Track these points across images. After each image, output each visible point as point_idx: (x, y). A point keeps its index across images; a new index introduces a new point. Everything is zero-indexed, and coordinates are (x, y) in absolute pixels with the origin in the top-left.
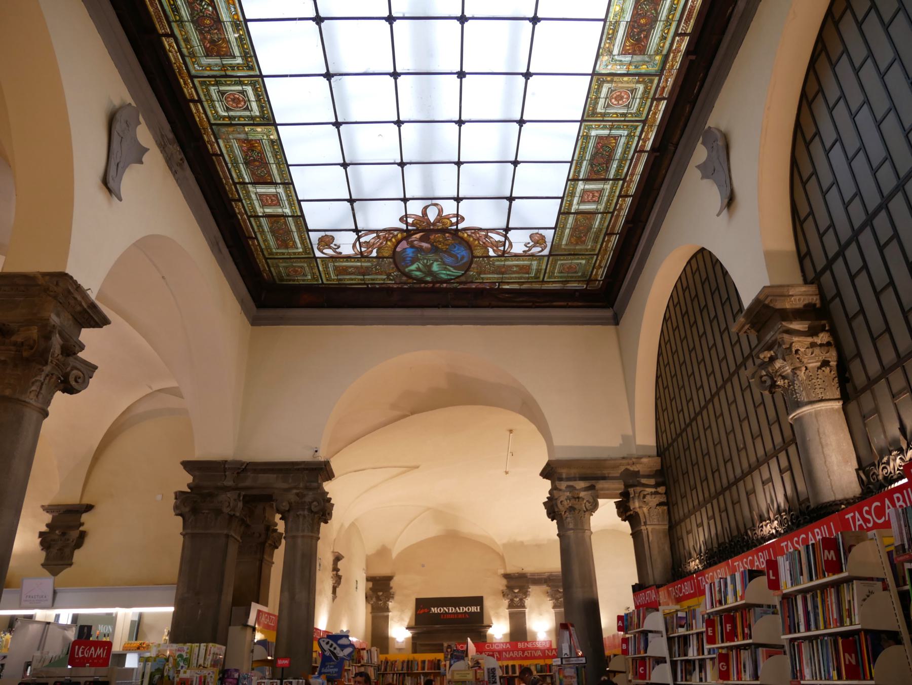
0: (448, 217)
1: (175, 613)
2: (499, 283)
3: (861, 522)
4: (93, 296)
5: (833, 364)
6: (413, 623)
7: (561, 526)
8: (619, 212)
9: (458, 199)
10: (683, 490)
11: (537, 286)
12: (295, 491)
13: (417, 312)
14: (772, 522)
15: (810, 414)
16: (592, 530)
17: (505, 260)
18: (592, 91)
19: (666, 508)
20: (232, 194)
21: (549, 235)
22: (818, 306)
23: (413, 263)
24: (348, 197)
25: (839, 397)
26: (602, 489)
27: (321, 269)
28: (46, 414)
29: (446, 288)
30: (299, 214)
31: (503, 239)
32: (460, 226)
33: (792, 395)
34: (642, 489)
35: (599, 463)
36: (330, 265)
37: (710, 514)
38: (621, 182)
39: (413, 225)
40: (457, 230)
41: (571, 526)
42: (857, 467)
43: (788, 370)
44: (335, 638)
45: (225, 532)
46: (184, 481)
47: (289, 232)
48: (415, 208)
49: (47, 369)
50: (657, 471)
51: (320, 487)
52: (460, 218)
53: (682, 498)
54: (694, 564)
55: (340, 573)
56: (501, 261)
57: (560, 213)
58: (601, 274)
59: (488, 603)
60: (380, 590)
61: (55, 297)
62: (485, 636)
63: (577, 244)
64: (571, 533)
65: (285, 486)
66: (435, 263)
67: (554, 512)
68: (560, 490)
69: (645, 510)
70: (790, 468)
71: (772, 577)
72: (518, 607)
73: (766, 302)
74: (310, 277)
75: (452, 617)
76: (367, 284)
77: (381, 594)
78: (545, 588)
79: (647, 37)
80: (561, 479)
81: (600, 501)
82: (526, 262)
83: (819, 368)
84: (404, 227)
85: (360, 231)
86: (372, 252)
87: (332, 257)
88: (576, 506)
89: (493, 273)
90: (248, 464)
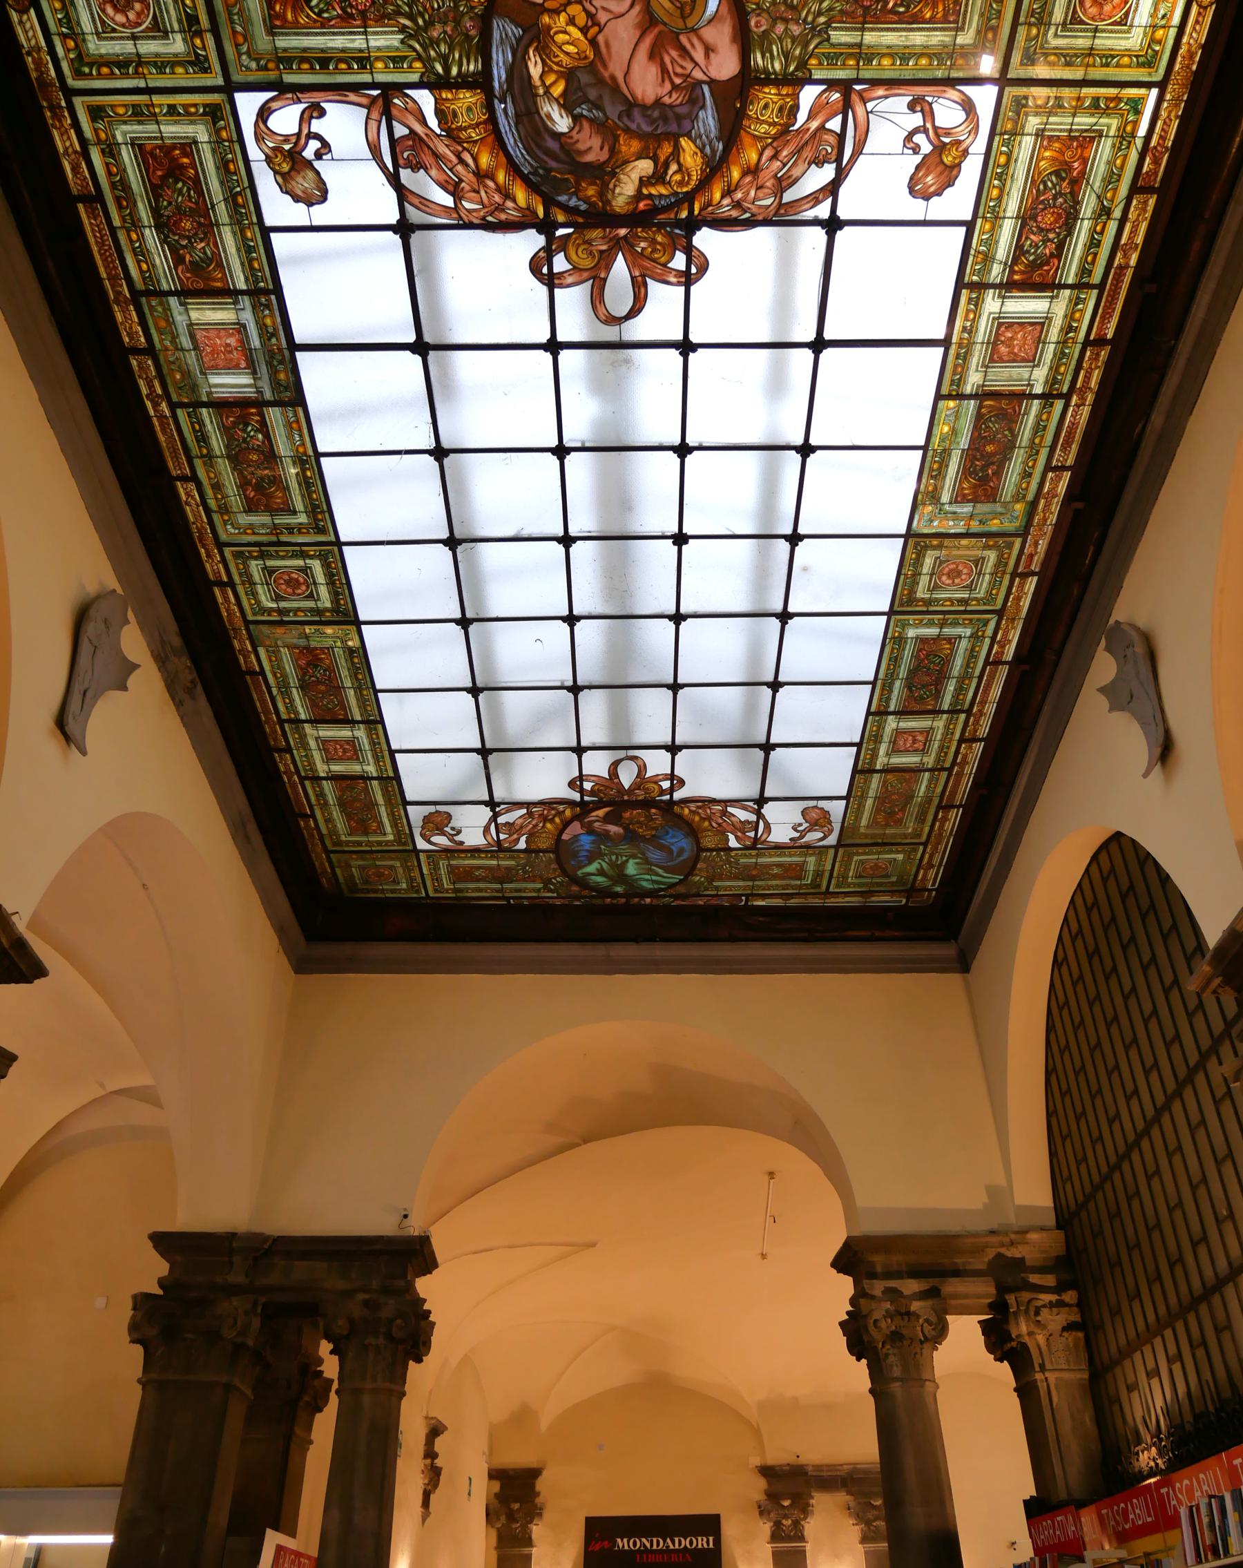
0: (655, 780)
2: (747, 896)
7: (876, 1373)
9: (673, 749)
11: (815, 902)
12: (362, 1296)
13: (598, 951)
17: (757, 856)
18: (907, 563)
21: (837, 809)
24: (479, 745)
30: (391, 774)
31: (753, 818)
32: (677, 795)
36: (443, 864)
37: (1172, 1350)
38: (963, 716)
39: (592, 793)
40: (671, 802)
46: (150, 1272)
47: (372, 805)
48: (597, 764)
50: (1058, 1258)
56: (751, 856)
57: (855, 771)
58: (932, 878)
59: (729, 1530)
63: (887, 825)
65: (341, 1285)
66: (631, 862)
68: (873, 1297)
69: (1041, 1339)
76: (508, 899)
77: (516, 1506)
78: (842, 1497)
79: (998, 474)
80: (873, 1276)
84: (576, 796)
85: (499, 804)
88: (905, 1332)
89: (736, 878)
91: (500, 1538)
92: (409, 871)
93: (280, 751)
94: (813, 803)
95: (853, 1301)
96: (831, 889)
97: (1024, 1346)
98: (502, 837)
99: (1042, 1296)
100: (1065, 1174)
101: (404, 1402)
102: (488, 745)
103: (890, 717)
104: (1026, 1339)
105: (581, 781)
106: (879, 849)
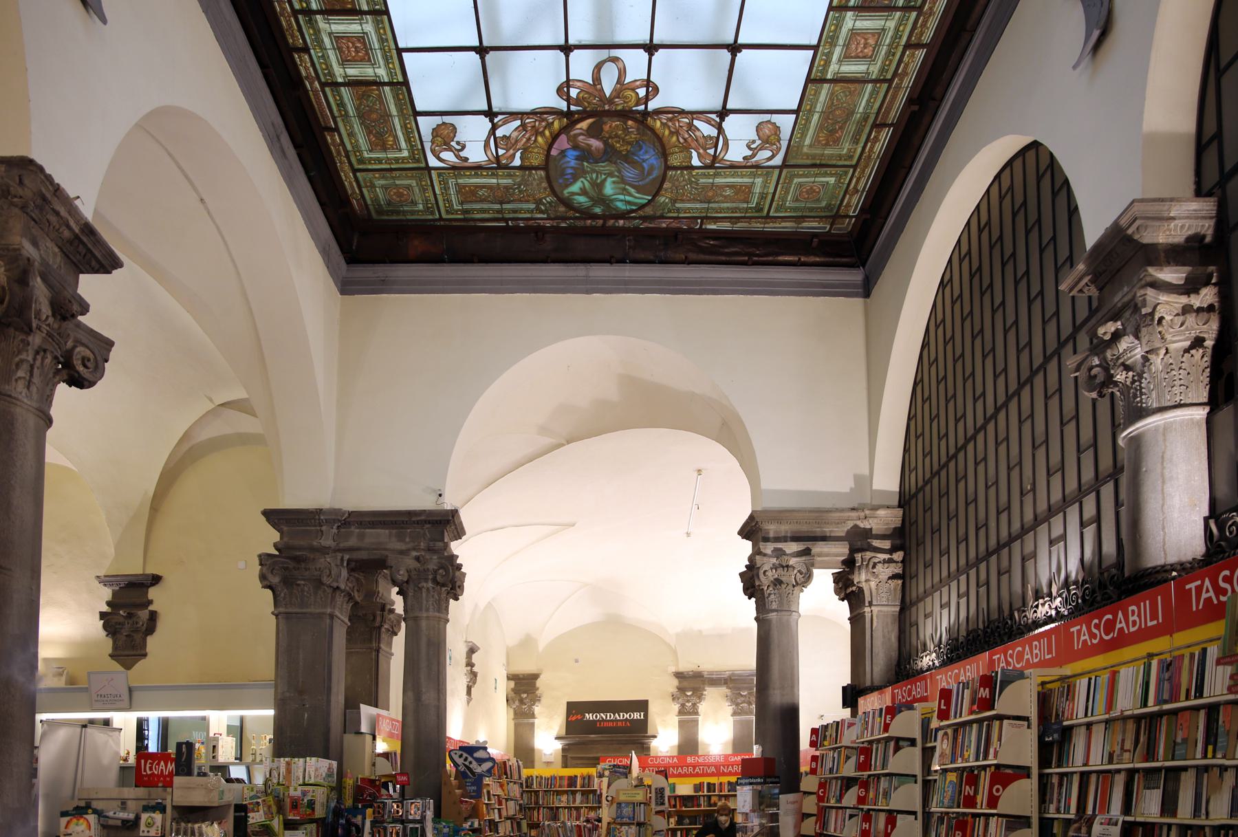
0: (633, 87)
1: (277, 719)
2: (702, 218)
3: (1087, 637)
4: (87, 211)
5: (1209, 343)
6: (563, 733)
7: (761, 608)
8: (901, 80)
9: (651, 48)
10: (928, 557)
11: (757, 226)
12: (414, 554)
13: (579, 271)
14: (1052, 598)
15: (1156, 429)
16: (801, 610)
17: (715, 175)
19: (900, 582)
20: (293, 36)
22: (1208, 239)
23: (575, 180)
24: (477, 44)
25: (1206, 400)
26: (820, 555)
27: (438, 192)
28: (49, 422)
29: (623, 229)
30: (401, 79)
31: (714, 132)
32: (653, 105)
33: (1135, 396)
34: (872, 554)
35: (820, 514)
36: (451, 182)
37: (963, 589)
38: (914, 14)
39: (578, 102)
40: (646, 113)
41: (774, 606)
42: (1207, 514)
43: (1138, 353)
44: (469, 750)
45: (329, 611)
46: (268, 539)
47: (387, 116)
49: (36, 340)
50: (895, 529)
51: (446, 546)
52: (652, 89)
53: (925, 567)
54: (927, 660)
55: (475, 669)
56: (708, 176)
57: (809, 80)
58: (855, 203)
59: (652, 709)
60: (524, 689)
61: (23, 208)
62: (648, 749)
63: (827, 144)
64: (773, 616)
65: (400, 546)
66: (610, 180)
67: (753, 586)
68: (765, 555)
69: (873, 584)
70: (1098, 519)
71: (943, 707)
72: (690, 714)
73: (1130, 232)
74: (421, 207)
75: (610, 724)
76: (506, 220)
77: (524, 696)
78: (724, 690)
80: (766, 540)
81: (816, 572)
82: (746, 180)
83: (1187, 351)
84: (563, 105)
86: (513, 156)
87: (454, 168)
88: (783, 579)
89: (694, 200)
90: (351, 514)
91: (515, 714)
92: (424, 190)
93: (299, 50)
94: (766, 117)
95: (751, 559)
96: (771, 214)
97: (861, 590)
98: (501, 152)
99: (880, 555)
100: (913, 465)
101: (448, 625)
102: (485, 44)
103: (850, 14)
104: (863, 585)
105: (568, 87)
106: (816, 170)
